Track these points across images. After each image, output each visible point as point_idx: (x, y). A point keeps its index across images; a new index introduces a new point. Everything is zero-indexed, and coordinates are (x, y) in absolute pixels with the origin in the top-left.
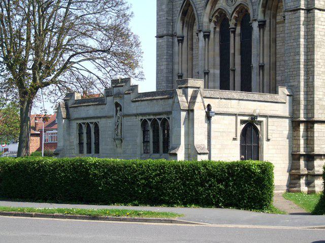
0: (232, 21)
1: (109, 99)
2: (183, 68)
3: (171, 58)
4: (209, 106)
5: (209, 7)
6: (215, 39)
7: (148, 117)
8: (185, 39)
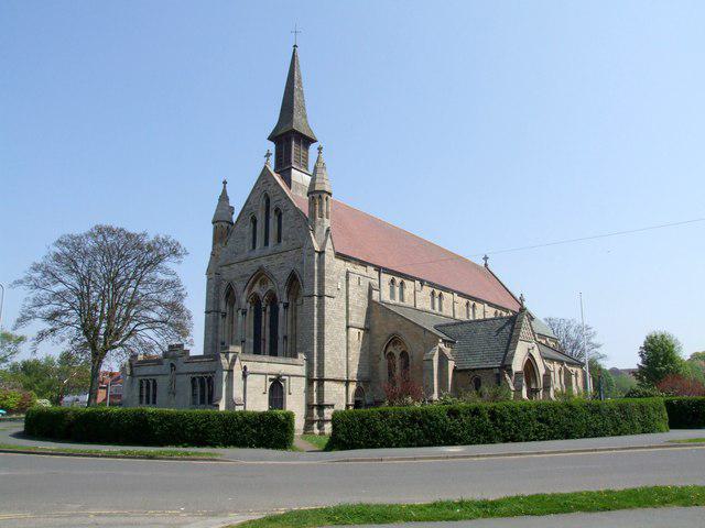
5: (246, 291)
6: (251, 315)
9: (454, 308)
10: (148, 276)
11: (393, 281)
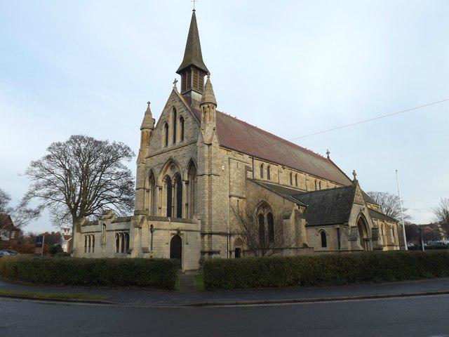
4: (152, 226)
5: (162, 174)
6: (165, 191)
9: (306, 183)
10: (109, 170)
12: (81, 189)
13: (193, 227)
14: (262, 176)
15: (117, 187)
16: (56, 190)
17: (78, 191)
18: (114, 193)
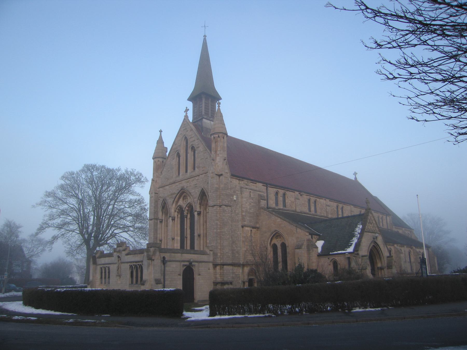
0: (185, 212)
1: (115, 254)
2: (162, 236)
3: (156, 231)
4: (164, 258)
5: (174, 204)
6: (178, 221)
7: (133, 264)
8: (164, 221)
10: (122, 197)
11: (277, 193)
12: (94, 218)
13: (204, 258)
14: (277, 204)
15: (130, 215)
16: (69, 219)
17: (92, 220)
18: (128, 221)
